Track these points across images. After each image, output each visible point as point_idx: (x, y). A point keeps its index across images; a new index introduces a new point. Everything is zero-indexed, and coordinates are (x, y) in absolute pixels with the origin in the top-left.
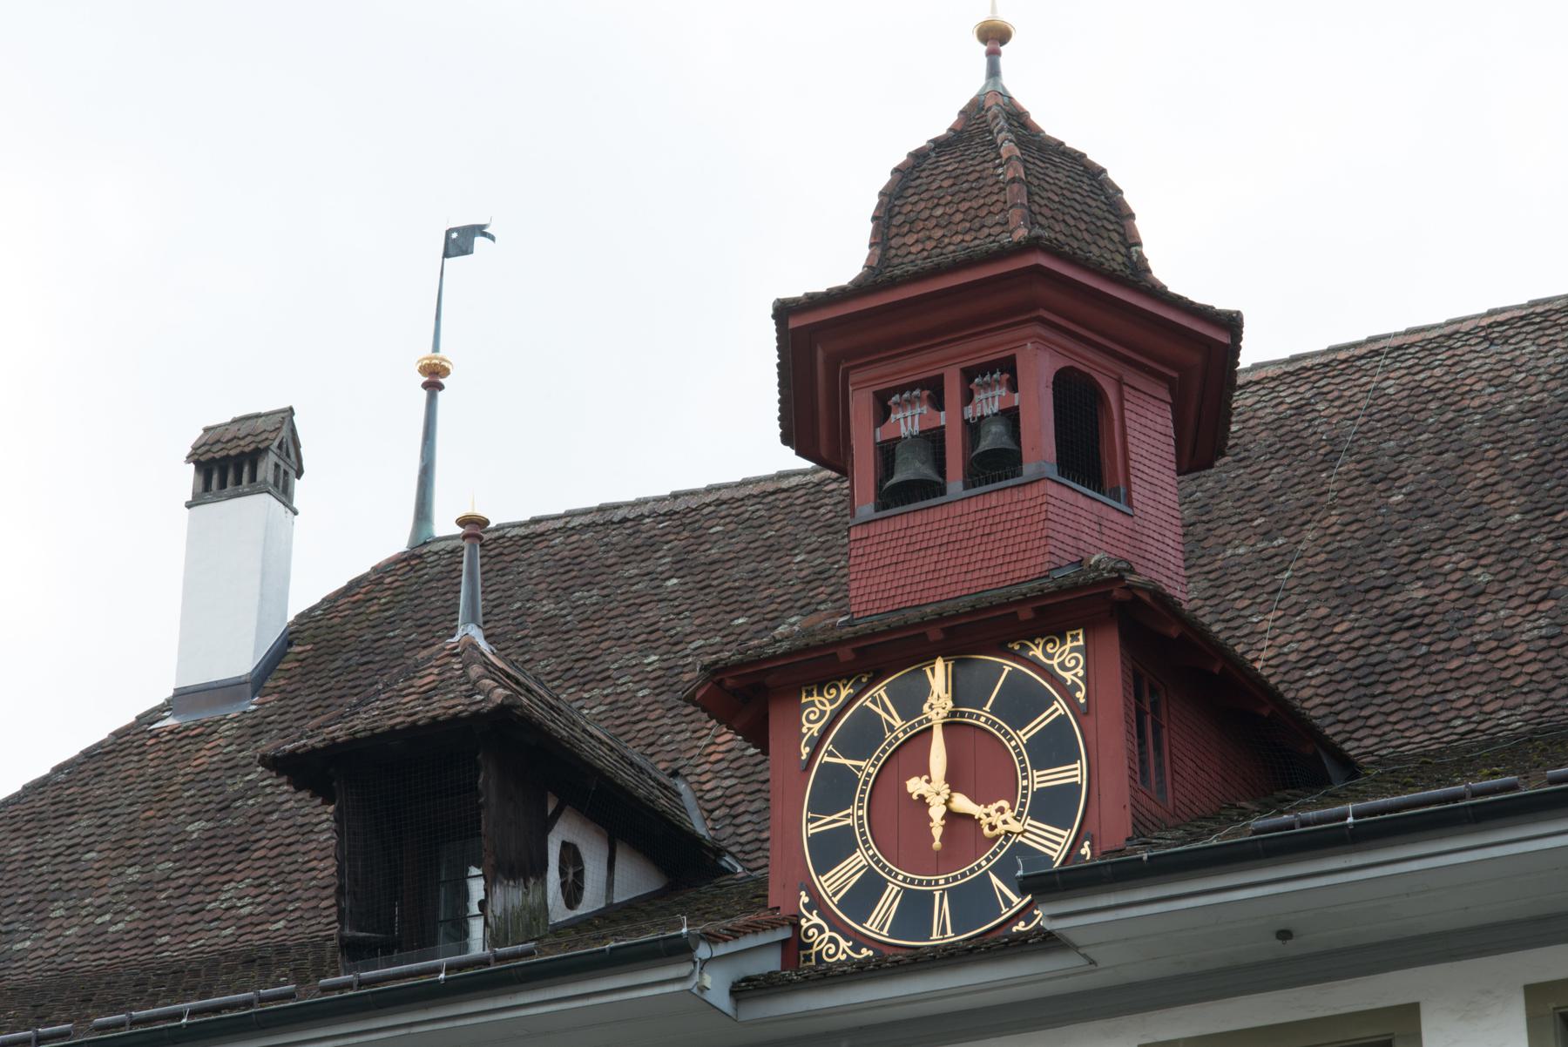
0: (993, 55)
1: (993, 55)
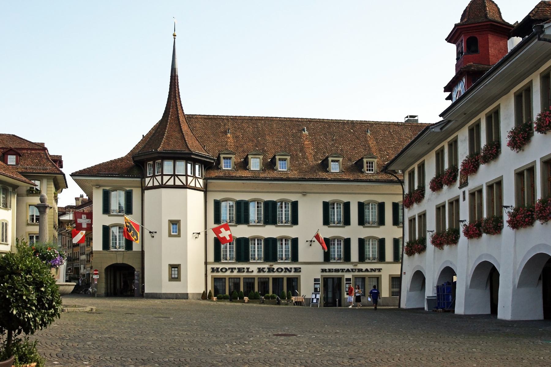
0: (175, 38)
1: (175, 38)
